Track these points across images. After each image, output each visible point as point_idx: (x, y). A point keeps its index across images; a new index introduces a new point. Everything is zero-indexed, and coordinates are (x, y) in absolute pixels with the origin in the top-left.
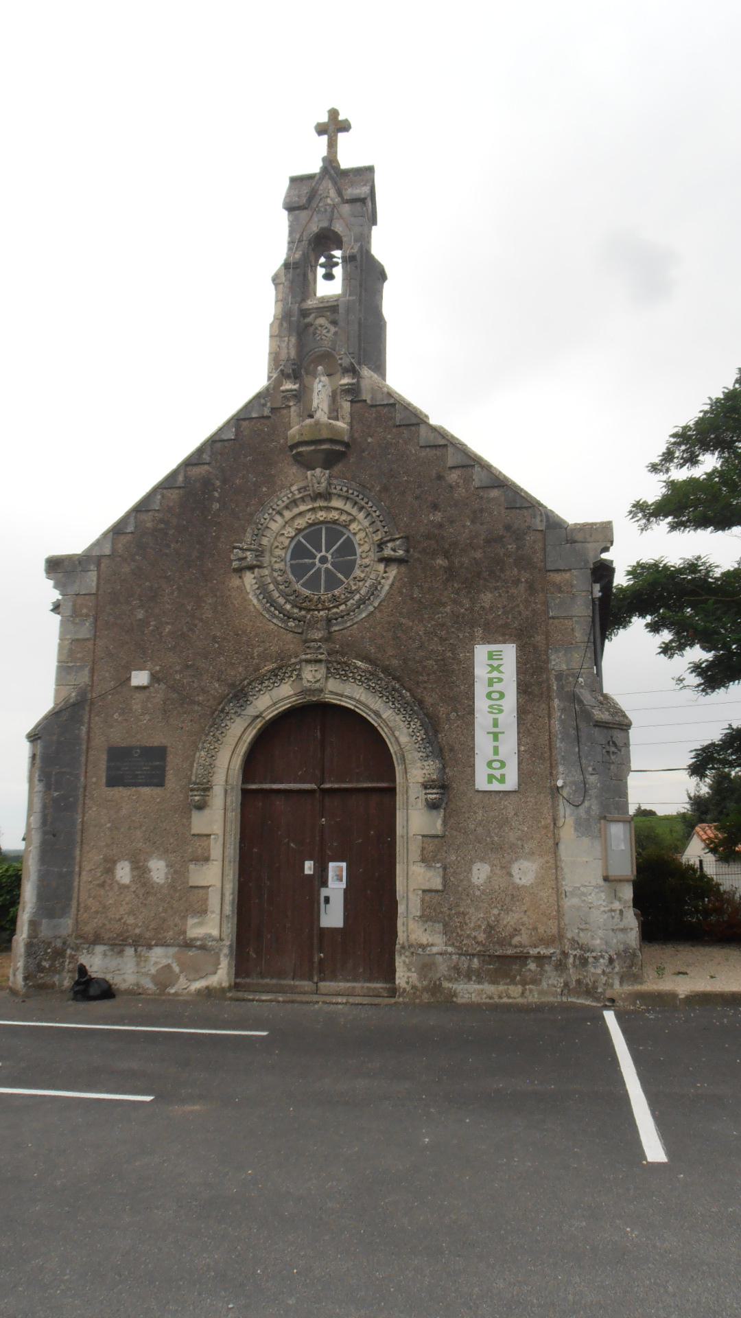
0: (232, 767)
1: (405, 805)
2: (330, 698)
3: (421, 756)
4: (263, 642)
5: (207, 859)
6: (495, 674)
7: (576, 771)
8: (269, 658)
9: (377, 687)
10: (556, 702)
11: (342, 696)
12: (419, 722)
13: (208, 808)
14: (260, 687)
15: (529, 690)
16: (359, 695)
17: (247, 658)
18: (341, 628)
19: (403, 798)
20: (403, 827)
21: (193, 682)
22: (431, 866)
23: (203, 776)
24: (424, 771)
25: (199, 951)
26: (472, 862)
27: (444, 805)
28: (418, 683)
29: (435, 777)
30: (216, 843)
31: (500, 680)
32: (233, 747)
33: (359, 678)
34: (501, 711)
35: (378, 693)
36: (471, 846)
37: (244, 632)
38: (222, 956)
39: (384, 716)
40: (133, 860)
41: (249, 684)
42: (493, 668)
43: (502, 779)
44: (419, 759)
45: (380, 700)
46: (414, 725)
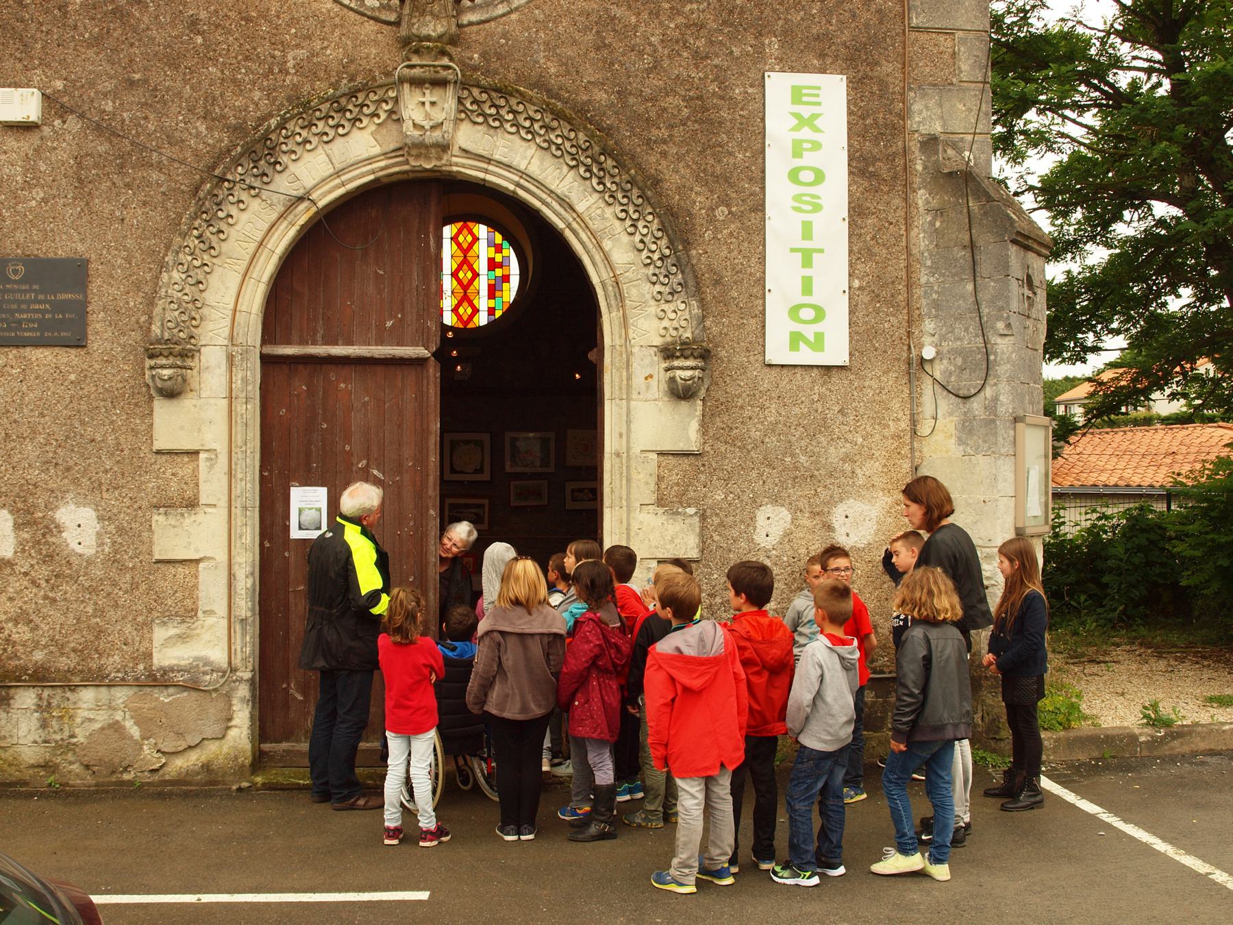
0: (243, 306)
1: (624, 391)
2: (463, 166)
3: (660, 293)
4: (309, 37)
5: (192, 504)
6: (806, 133)
7: (966, 330)
8: (322, 74)
9: (568, 145)
10: (921, 197)
11: (489, 161)
12: (656, 221)
13: (190, 395)
14: (304, 133)
15: (871, 169)
16: (526, 162)
17: (271, 71)
18: (484, 17)
19: (621, 376)
20: (621, 435)
21: (146, 118)
22: (679, 513)
23: (178, 325)
24: (666, 323)
25: (185, 694)
26: (756, 503)
27: (702, 393)
28: (648, 142)
29: (689, 335)
30: (211, 467)
31: (816, 146)
32: (245, 263)
33: (527, 124)
34: (817, 208)
35: (568, 158)
36: (754, 474)
37: (264, 15)
38: (235, 701)
39: (580, 208)
40: (20, 505)
41: (281, 126)
42: (802, 122)
43: (818, 343)
44: (653, 297)
45: (572, 172)
46: (645, 227)
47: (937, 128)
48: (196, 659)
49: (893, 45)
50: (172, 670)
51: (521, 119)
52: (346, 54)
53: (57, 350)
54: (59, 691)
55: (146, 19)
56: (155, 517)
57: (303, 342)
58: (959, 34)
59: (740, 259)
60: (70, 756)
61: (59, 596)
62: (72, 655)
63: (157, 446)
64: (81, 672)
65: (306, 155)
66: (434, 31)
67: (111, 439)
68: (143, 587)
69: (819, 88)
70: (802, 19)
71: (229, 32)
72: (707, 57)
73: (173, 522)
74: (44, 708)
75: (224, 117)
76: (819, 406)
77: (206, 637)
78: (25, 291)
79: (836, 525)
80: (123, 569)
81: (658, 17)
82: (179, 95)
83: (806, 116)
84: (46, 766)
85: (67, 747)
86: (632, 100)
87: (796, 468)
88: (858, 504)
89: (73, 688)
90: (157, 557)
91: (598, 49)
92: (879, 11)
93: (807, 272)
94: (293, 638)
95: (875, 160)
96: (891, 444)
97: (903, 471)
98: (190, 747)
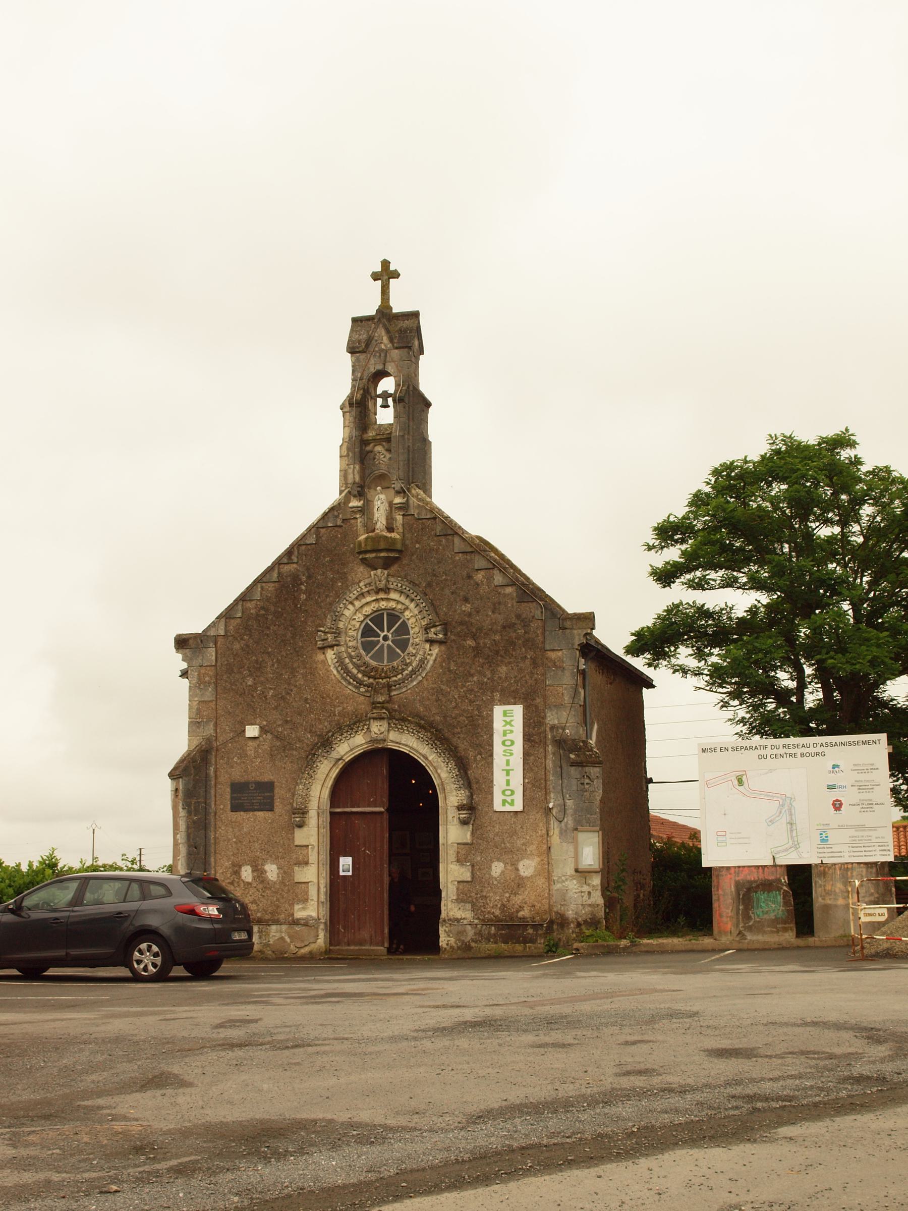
0: (322, 796)
4: (342, 703)
6: (508, 727)
10: (550, 748)
11: (400, 744)
24: (458, 798)
27: (472, 822)
31: (512, 732)
34: (512, 754)
36: (491, 850)
37: (328, 696)
39: (430, 758)
41: (333, 735)
42: (507, 723)
43: (512, 803)
47: (556, 722)
51: (409, 729)
57: (344, 807)
58: (564, 686)
61: (265, 894)
63: (296, 843)
67: (281, 842)
71: (317, 703)
75: (316, 732)
76: (513, 826)
77: (311, 908)
82: (302, 725)
83: (508, 721)
86: (448, 719)
89: (269, 925)
91: (437, 701)
93: (508, 778)
95: (533, 735)
96: (540, 839)
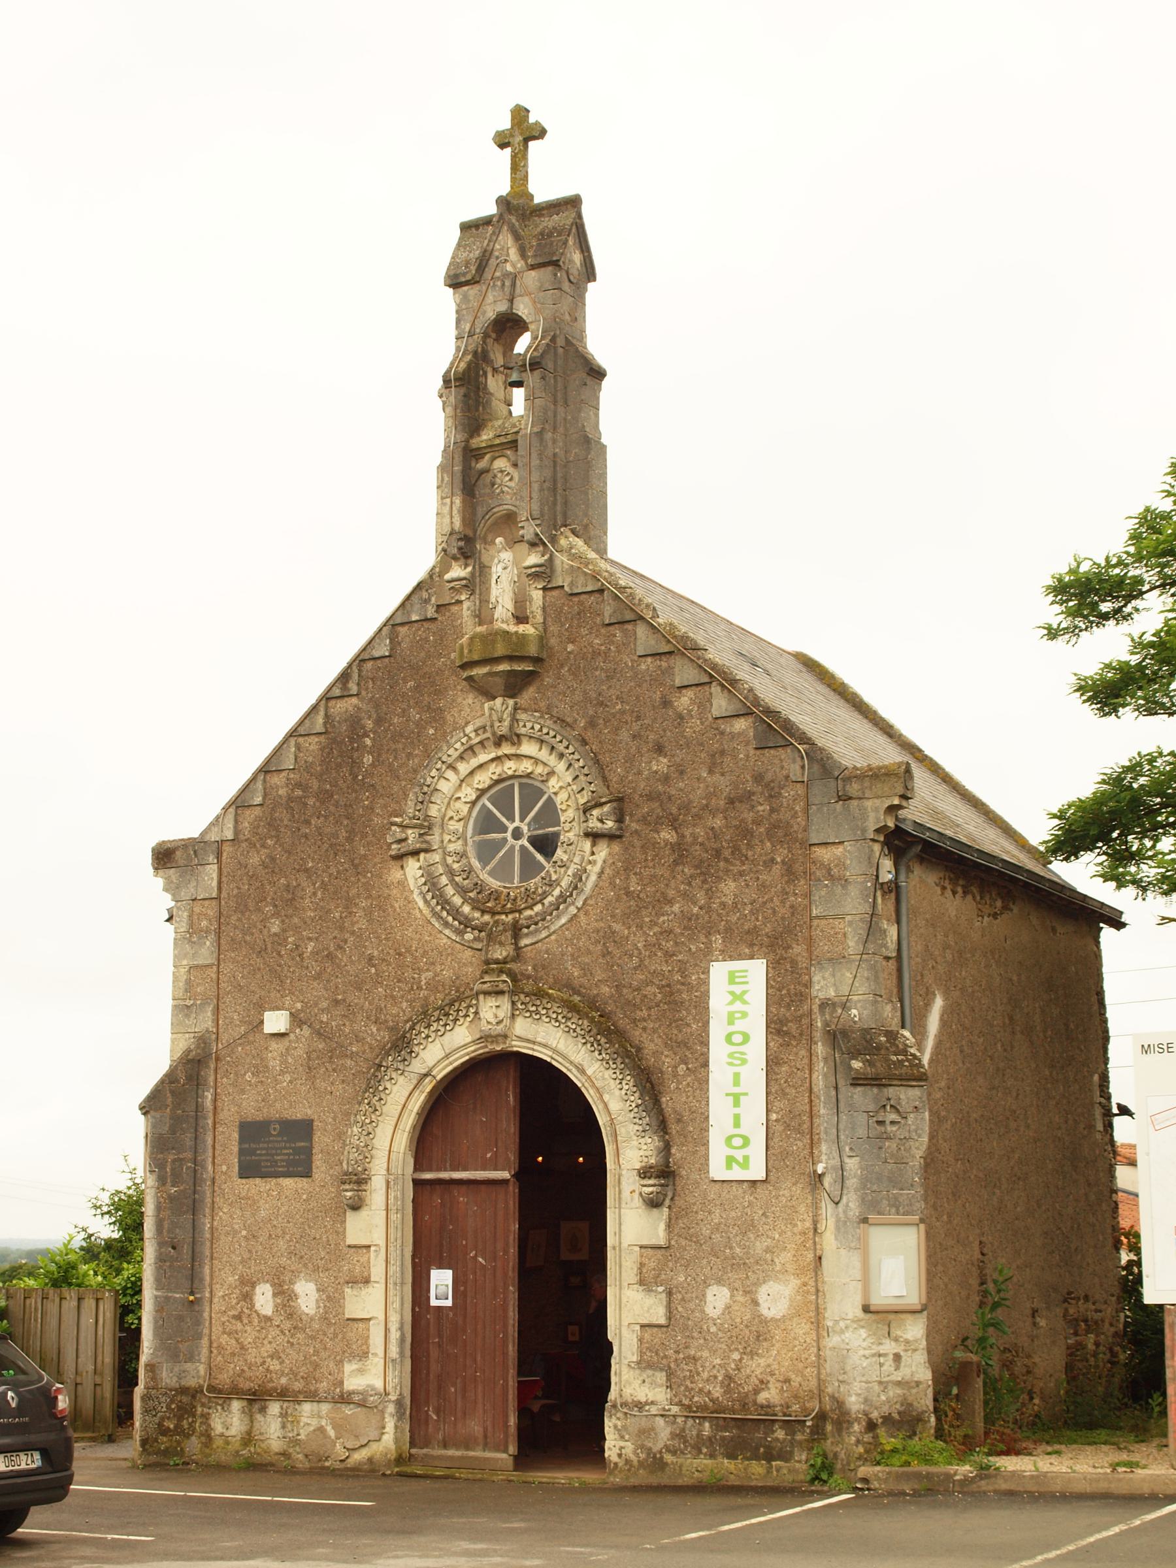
0: (394, 1148)
2: (519, 1047)
5: (367, 1281)
6: (738, 1006)
11: (534, 1043)
15: (785, 1029)
16: (556, 1042)
17: (412, 989)
18: (535, 940)
21: (344, 1025)
22: (652, 1291)
23: (357, 1162)
27: (667, 1202)
28: (634, 1021)
30: (377, 1256)
31: (745, 1015)
32: (396, 1119)
34: (744, 1062)
36: (705, 1262)
37: (408, 951)
38: (386, 1416)
39: (589, 1072)
40: (276, 1281)
41: (412, 1028)
43: (745, 1164)
47: (832, 993)
48: (368, 1386)
49: (801, 932)
50: (354, 1393)
52: (454, 974)
53: (296, 1179)
54: (292, 1403)
55: (345, 959)
56: (346, 1290)
59: (695, 1103)
60: (298, 1449)
61: (295, 1341)
62: (301, 1381)
63: (349, 1241)
64: (306, 1392)
65: (429, 1045)
66: (501, 954)
68: (340, 1336)
69: (747, 971)
70: (738, 919)
72: (674, 955)
73: (355, 1293)
74: (284, 1415)
75: (386, 1021)
76: (748, 1210)
78: (279, 1142)
79: (761, 1301)
80: (330, 1324)
81: (642, 929)
84: (285, 1454)
85: (295, 1442)
86: (625, 991)
87: (733, 1258)
88: (776, 1285)
89: (299, 1402)
90: (347, 1316)
92: (792, 907)
93: (737, 1111)
94: (432, 1376)
95: (788, 1021)
96: (799, 1239)
97: (808, 1260)
98: (362, 1446)
